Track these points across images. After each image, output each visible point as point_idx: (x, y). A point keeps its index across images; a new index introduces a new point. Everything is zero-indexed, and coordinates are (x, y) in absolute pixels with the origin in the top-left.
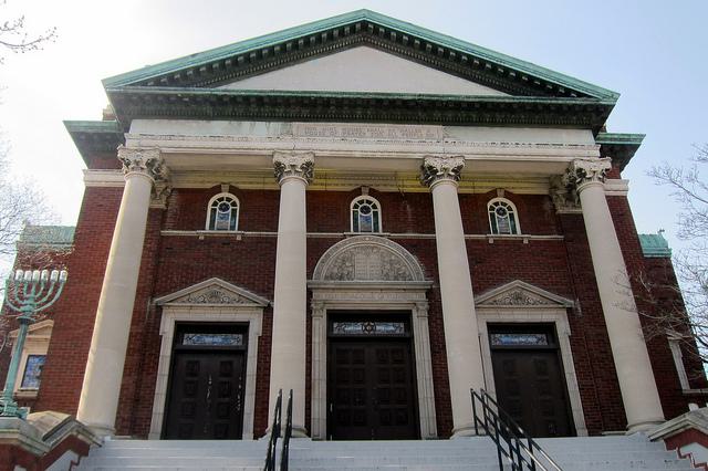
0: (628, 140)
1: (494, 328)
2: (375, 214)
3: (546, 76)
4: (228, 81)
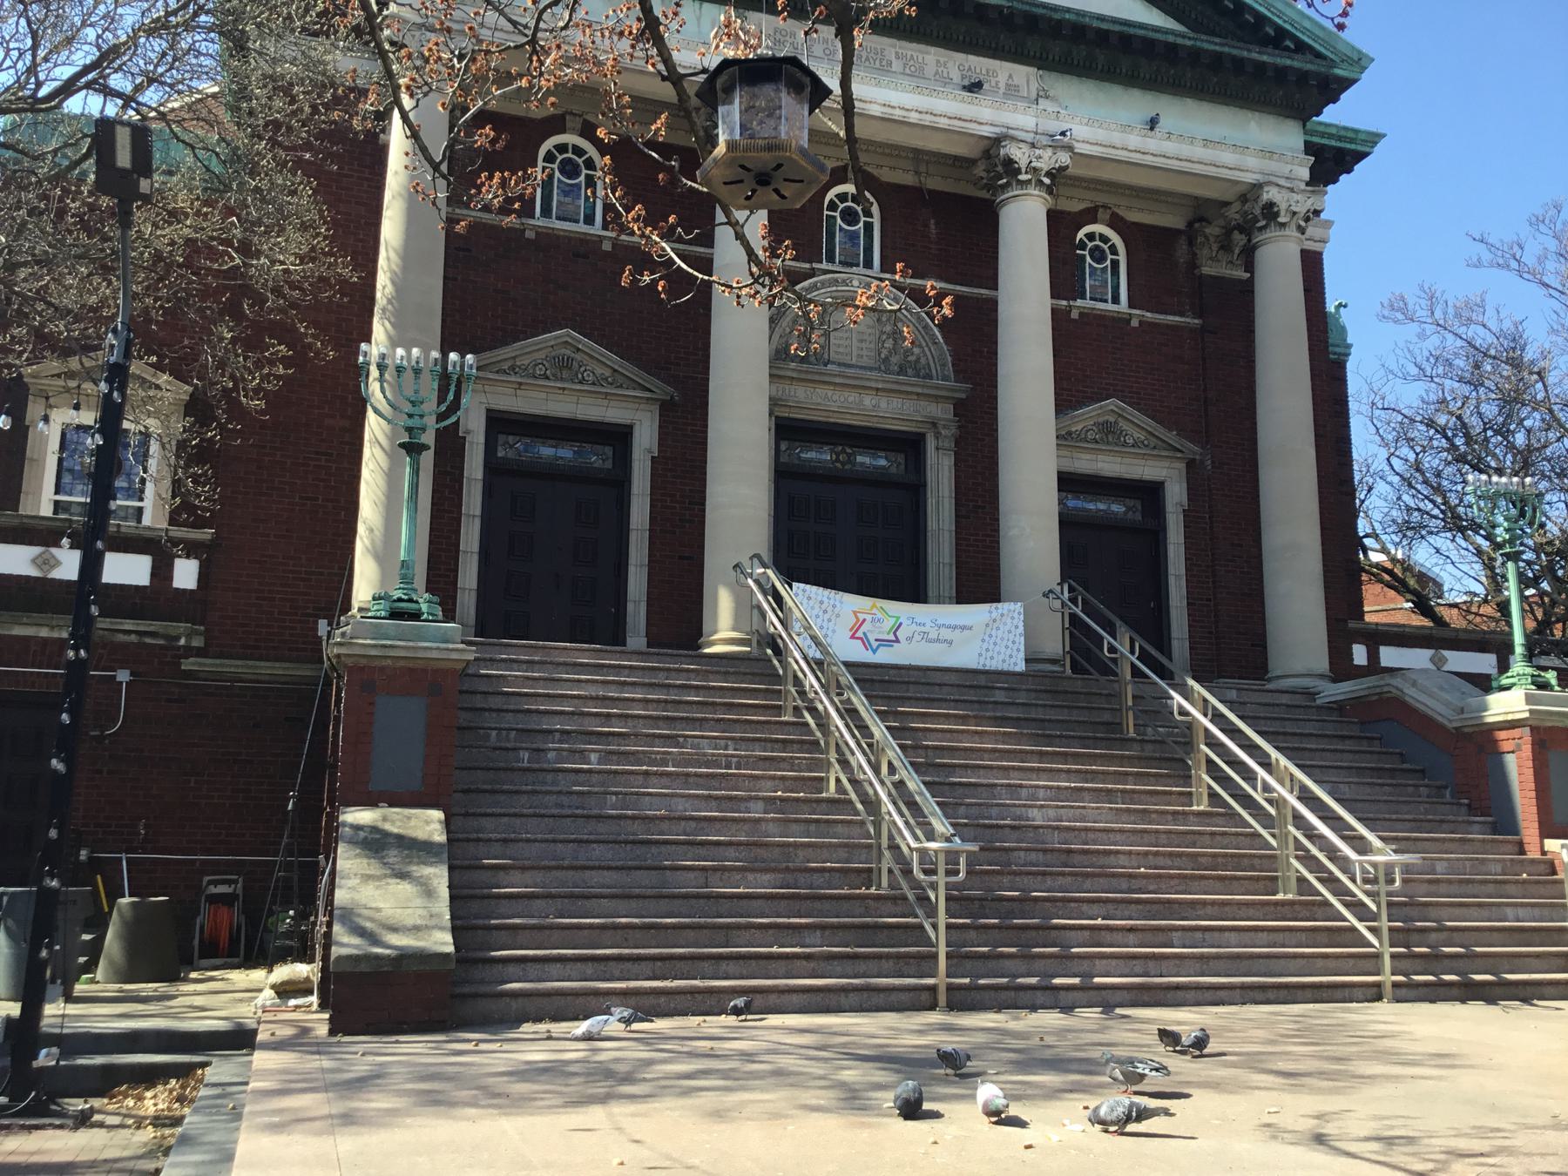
0: (1352, 141)
1: (1068, 482)
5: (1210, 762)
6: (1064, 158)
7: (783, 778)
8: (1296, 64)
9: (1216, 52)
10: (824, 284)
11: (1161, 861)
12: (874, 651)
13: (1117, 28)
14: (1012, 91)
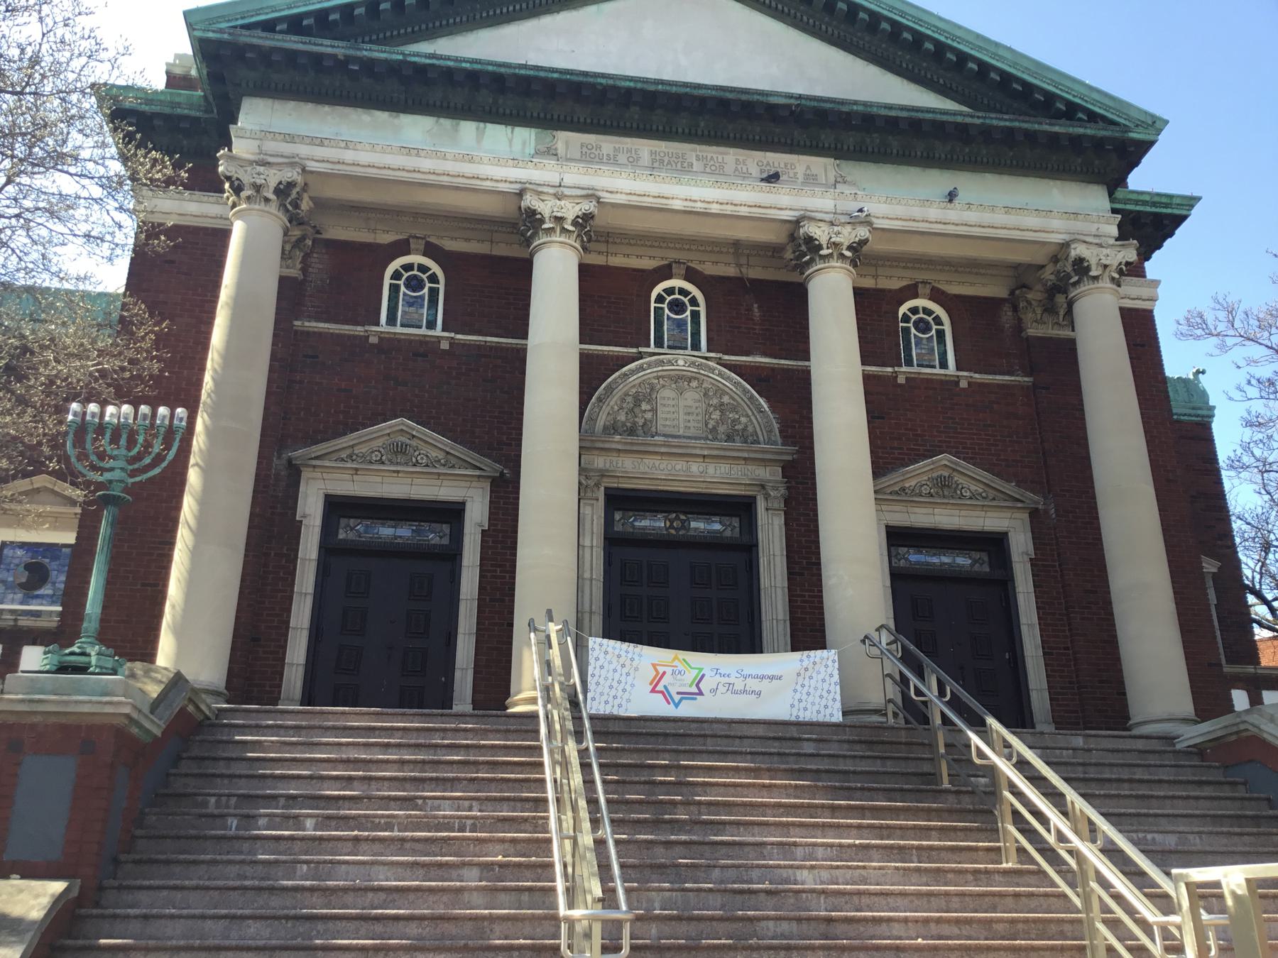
0: (1167, 206)
1: (897, 537)
2: (695, 315)
3: (1014, 65)
4: (431, 35)
5: (1016, 813)
6: (863, 232)
7: (513, 841)
8: (1089, 132)
9: (1007, 127)
10: (650, 365)
11: (946, 929)
12: (677, 705)
13: (904, 114)
14: (811, 179)
